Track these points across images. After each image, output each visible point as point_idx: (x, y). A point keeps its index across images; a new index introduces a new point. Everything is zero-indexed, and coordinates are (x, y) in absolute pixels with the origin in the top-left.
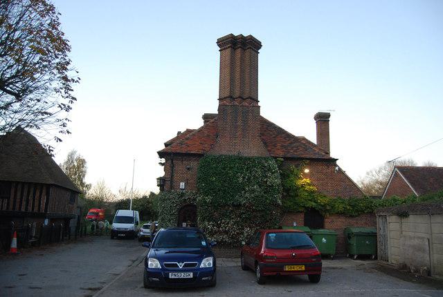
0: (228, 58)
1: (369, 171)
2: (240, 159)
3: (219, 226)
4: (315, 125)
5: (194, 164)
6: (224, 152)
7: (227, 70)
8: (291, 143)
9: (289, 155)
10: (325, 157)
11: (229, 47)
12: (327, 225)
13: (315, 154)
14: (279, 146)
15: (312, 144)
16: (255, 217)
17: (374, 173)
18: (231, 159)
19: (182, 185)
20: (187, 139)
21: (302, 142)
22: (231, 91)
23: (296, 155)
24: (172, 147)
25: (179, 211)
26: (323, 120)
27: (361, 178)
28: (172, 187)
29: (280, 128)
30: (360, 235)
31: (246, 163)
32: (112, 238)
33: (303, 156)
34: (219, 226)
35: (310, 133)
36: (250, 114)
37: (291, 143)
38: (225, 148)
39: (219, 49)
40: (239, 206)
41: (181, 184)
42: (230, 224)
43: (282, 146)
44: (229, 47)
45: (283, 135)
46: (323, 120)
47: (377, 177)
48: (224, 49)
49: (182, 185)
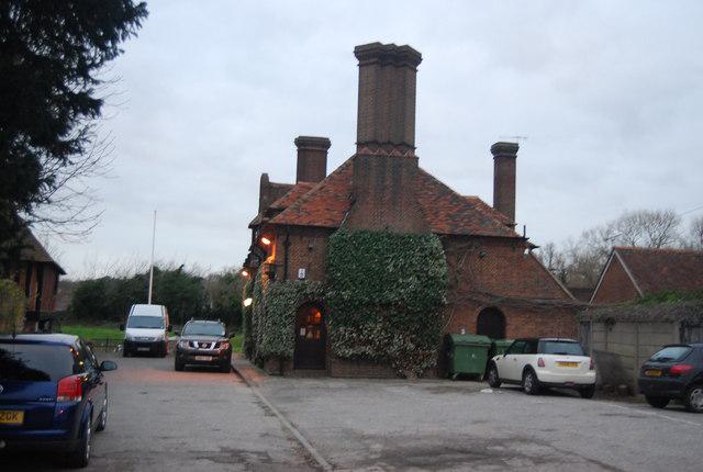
1: (587, 229)
2: (389, 236)
3: (360, 332)
5: (317, 243)
6: (365, 226)
8: (461, 211)
9: (458, 231)
10: (511, 235)
11: (373, 63)
13: (495, 230)
14: (442, 213)
15: (485, 206)
16: (411, 321)
17: (598, 236)
18: (377, 237)
20: (305, 201)
23: (469, 230)
24: (285, 215)
25: (298, 310)
26: (505, 155)
27: (571, 243)
28: (286, 276)
30: (593, 461)
31: (403, 243)
33: (478, 233)
34: (360, 332)
35: (476, 183)
38: (370, 220)
40: (388, 305)
42: (375, 329)
43: (448, 215)
44: (373, 63)
45: (449, 197)
46: (505, 155)
47: (603, 244)
48: (367, 65)
49: (302, 272)
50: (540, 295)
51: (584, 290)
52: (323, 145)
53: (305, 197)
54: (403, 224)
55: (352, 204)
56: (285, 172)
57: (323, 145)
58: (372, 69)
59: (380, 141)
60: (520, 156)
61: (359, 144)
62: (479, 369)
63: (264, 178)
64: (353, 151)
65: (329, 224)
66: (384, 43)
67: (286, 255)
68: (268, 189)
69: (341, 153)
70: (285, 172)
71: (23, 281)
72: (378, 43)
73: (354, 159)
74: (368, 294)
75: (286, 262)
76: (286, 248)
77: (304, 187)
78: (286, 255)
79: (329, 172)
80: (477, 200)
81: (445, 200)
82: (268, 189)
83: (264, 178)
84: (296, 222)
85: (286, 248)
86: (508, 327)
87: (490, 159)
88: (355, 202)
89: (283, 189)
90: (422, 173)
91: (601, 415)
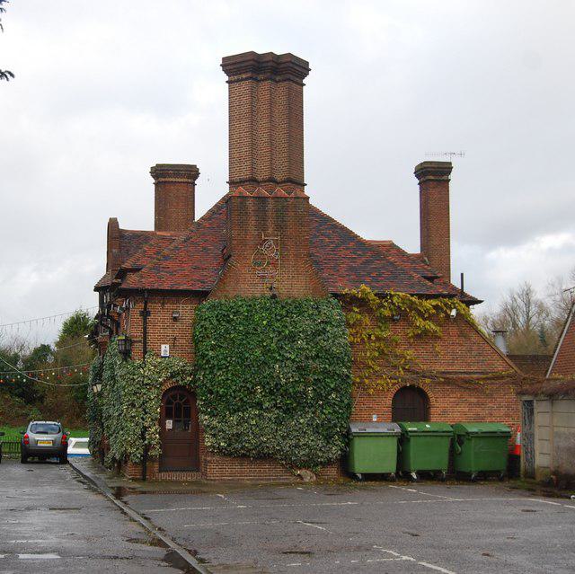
0: (246, 99)
4: (417, 188)
5: (186, 310)
7: (245, 124)
12: (433, 419)
19: (165, 349)
21: (384, 252)
22: (252, 168)
26: (433, 178)
29: (343, 229)
32: (24, 461)
36: (476, 400)
37: (367, 262)
39: (227, 78)
41: (163, 346)
43: (351, 269)
44: (246, 79)
46: (433, 178)
48: (238, 81)
49: (165, 349)
50: (474, 368)
51: (535, 358)
52: (191, 173)
53: (166, 251)
54: (293, 284)
55: (226, 260)
56: (140, 216)
57: (191, 173)
58: (246, 86)
59: (259, 178)
60: (455, 179)
61: (231, 183)
62: (390, 467)
63: (113, 224)
64: (225, 190)
65: (198, 287)
66: (260, 52)
67: (145, 328)
68: (117, 236)
69: (209, 193)
70: (140, 216)
71: (533, 309)
72: (252, 53)
73: (227, 200)
74: (500, 407)
75: (145, 338)
76: (145, 319)
77: (163, 238)
78: (145, 328)
79: (197, 218)
80: (391, 247)
81: (347, 249)
82: (117, 236)
83: (113, 224)
84: (156, 286)
85: (145, 319)
86: (432, 410)
87: (414, 184)
88: (230, 256)
89: (139, 237)
90: (316, 213)
91: (523, 511)
